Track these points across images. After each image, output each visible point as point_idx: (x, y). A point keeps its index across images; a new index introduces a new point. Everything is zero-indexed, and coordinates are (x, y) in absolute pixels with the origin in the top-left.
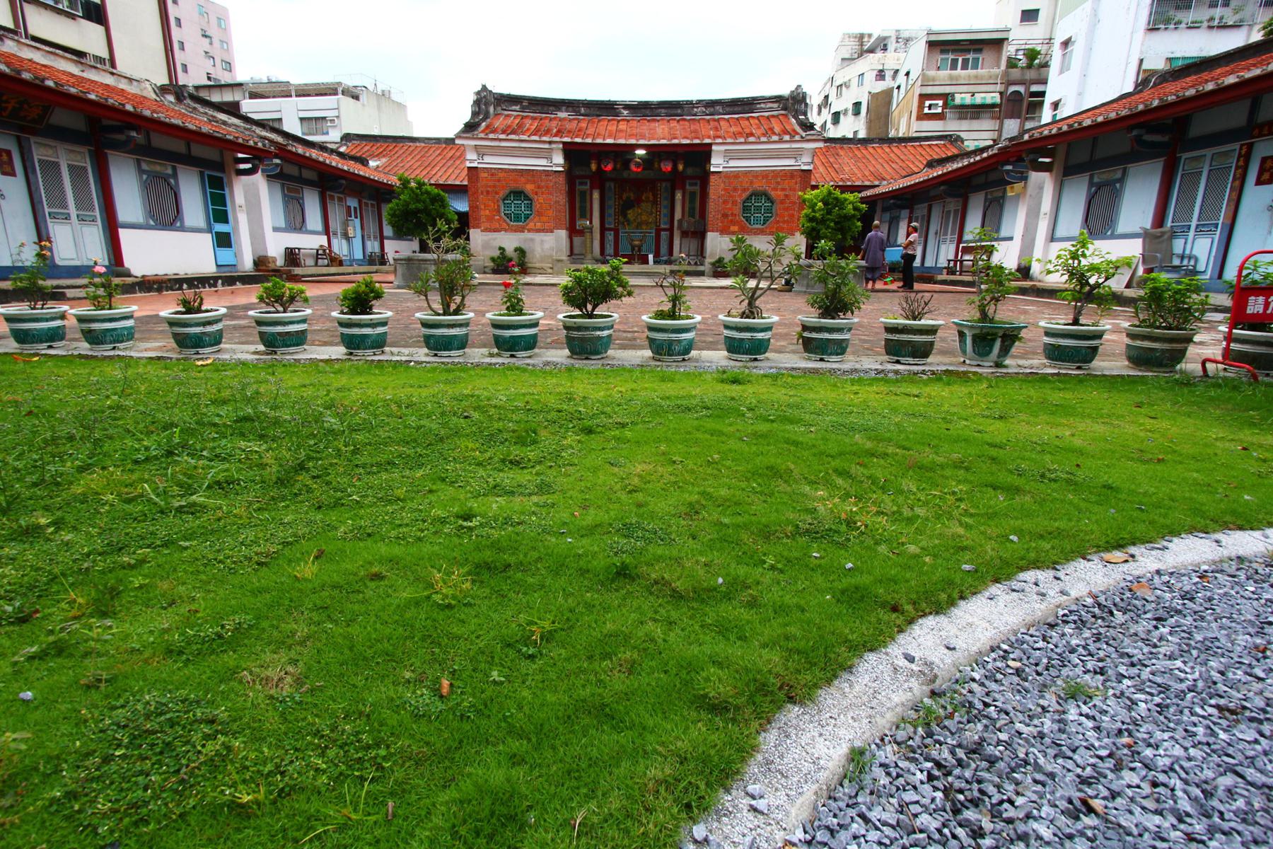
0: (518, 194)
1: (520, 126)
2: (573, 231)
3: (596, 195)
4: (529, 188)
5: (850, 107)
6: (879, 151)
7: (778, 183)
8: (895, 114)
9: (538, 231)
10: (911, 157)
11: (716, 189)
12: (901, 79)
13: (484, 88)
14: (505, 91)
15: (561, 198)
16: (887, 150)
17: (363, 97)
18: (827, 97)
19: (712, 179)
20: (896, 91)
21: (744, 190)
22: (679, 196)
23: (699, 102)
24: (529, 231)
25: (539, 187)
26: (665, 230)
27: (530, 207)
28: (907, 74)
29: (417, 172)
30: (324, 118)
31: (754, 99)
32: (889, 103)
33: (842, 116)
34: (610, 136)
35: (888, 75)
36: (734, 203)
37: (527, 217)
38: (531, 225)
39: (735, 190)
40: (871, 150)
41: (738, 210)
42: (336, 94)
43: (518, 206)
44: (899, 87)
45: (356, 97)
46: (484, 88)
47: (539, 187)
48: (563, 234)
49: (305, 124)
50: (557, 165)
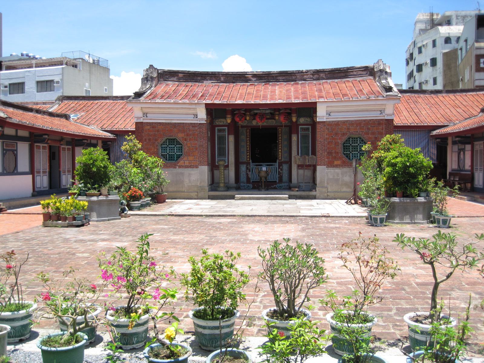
0: (172, 141)
1: (175, 92)
2: (213, 167)
3: (232, 138)
4: (180, 136)
5: (429, 62)
6: (447, 98)
7: (368, 129)
8: (461, 66)
9: (187, 167)
10: (470, 103)
11: (321, 135)
12: (462, 44)
13: (151, 66)
14: (167, 68)
15: (203, 143)
16: (453, 98)
17: (80, 67)
18: (412, 55)
19: (318, 127)
20: (459, 52)
21: (344, 134)
22: (294, 138)
23: (307, 72)
24: (180, 167)
25: (187, 135)
26: (285, 162)
27: (181, 149)
28: (466, 41)
29: (105, 122)
30: (52, 81)
31: (348, 69)
32: (456, 58)
33: (423, 67)
34: (240, 98)
35: (453, 41)
36: (337, 144)
37: (179, 157)
38: (181, 162)
39: (336, 134)
40: (441, 98)
41: (340, 149)
42: (62, 64)
43: (172, 149)
44: (461, 49)
45: (75, 66)
46: (151, 66)
47: (187, 135)
48: (205, 169)
49: (39, 85)
50: (202, 119)
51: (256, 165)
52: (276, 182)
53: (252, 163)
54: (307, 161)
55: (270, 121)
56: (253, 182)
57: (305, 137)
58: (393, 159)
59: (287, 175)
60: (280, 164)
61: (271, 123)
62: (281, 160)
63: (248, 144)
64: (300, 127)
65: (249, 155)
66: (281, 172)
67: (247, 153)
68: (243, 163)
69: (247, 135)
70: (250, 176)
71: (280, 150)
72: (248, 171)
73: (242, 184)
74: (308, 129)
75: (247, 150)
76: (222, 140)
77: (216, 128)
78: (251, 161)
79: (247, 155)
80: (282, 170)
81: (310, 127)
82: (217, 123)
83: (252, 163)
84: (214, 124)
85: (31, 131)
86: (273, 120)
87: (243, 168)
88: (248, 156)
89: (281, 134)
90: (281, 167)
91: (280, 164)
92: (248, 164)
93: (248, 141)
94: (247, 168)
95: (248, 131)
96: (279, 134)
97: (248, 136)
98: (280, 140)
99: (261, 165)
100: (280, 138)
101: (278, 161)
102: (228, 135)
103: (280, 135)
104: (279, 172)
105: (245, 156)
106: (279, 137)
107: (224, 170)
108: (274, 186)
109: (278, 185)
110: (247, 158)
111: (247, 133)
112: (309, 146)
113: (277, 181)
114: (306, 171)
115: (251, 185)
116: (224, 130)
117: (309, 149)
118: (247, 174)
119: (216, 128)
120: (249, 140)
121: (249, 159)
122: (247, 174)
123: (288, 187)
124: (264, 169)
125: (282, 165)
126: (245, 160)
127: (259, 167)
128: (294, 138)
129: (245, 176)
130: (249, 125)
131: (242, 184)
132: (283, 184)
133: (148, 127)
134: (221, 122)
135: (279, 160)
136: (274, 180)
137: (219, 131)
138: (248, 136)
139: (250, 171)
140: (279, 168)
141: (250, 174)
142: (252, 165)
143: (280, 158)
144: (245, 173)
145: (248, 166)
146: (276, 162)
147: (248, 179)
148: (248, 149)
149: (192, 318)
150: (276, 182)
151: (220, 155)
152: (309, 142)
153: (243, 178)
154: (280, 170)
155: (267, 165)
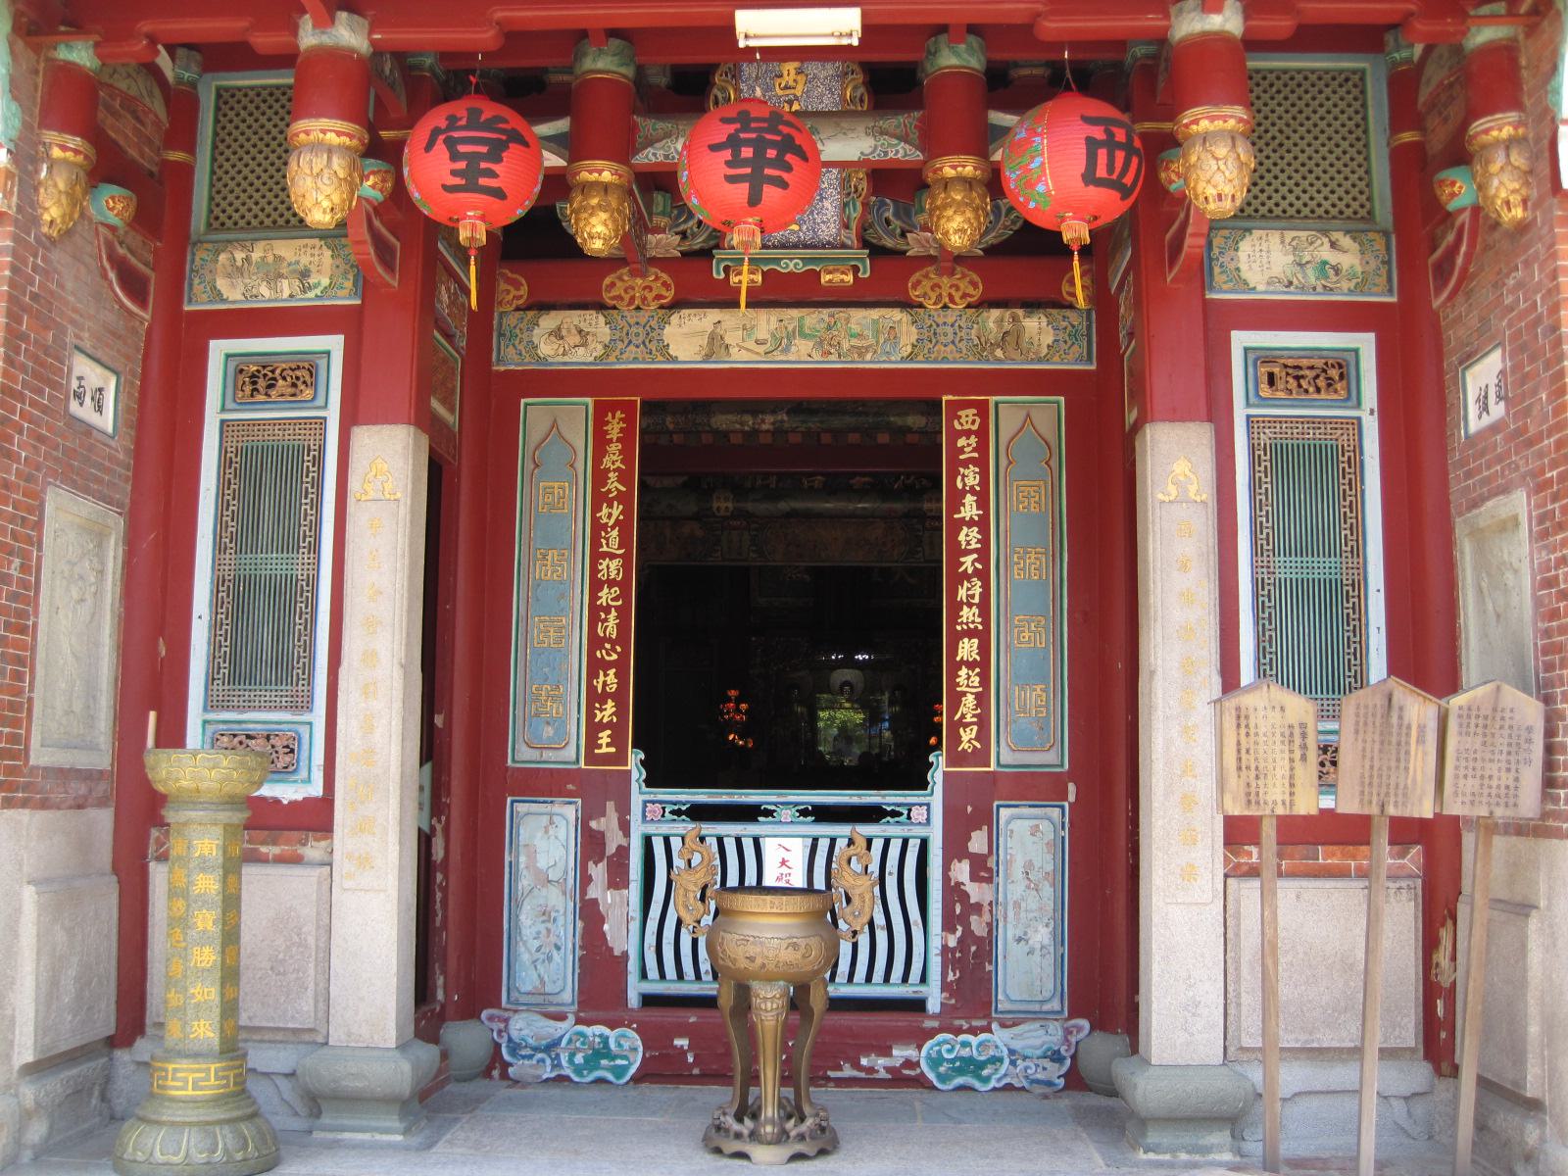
3: (382, 478)
22: (1175, 468)
51: (698, 813)
52: (917, 1005)
53: (650, 782)
54: (1422, 761)
55: (861, 319)
56: (648, 1000)
57: (1303, 469)
58: (20, 870)
59: (1042, 935)
60: (969, 814)
61: (876, 341)
62: (981, 756)
63: (611, 568)
64: (1241, 340)
65: (619, 697)
66: (976, 892)
67: (595, 666)
68: (545, 784)
69: (600, 477)
70: (622, 933)
71: (968, 649)
72: (598, 871)
73: (526, 1027)
74: (1336, 373)
75: (596, 642)
76: (279, 486)
77: (219, 350)
78: (635, 758)
79: (595, 698)
80: (982, 869)
81: (1365, 343)
82: (234, 294)
83: (650, 782)
84: (198, 302)
85: (150, 741)
86: (896, 314)
87: (543, 841)
88: (607, 712)
89: (982, 463)
90: (978, 843)
91: (969, 814)
92: (594, 789)
93: (612, 541)
94: (591, 844)
95: (614, 429)
96: (956, 464)
97: (614, 485)
98: (969, 537)
99: (750, 813)
100: (969, 509)
101: (939, 763)
102: (351, 418)
103: (971, 477)
104: (953, 892)
105: (564, 682)
106: (956, 502)
107: (231, 868)
108: (900, 1053)
109: (942, 1044)
110: (594, 729)
111: (600, 450)
112: (1360, 584)
113: (934, 1006)
114: (1288, 891)
115: (629, 1045)
116: (304, 373)
117: (1360, 610)
118: (591, 915)
119: (219, 350)
120: (623, 525)
121: (617, 740)
122: (591, 915)
123: (1055, 1072)
124: (785, 852)
125: (985, 818)
126: (570, 753)
127: (729, 830)
128: (1181, 467)
129: (567, 930)
130: (632, 360)
131: (526, 1027)
132: (1000, 1037)
133: (570, 787)
134: (274, 277)
135: (957, 758)
136: (896, 990)
137: (255, 379)
138: (614, 485)
139: (618, 878)
140: (955, 848)
141: (620, 907)
142: (649, 812)
143: (968, 736)
144: (561, 903)
145: (607, 823)
146: (917, 780)
147: (600, 977)
148: (611, 626)
149: (1021, 123)
150: (917, 1005)
151: (238, 670)
152: (1358, 529)
153: (540, 949)
154: (962, 871)
155: (823, 814)
